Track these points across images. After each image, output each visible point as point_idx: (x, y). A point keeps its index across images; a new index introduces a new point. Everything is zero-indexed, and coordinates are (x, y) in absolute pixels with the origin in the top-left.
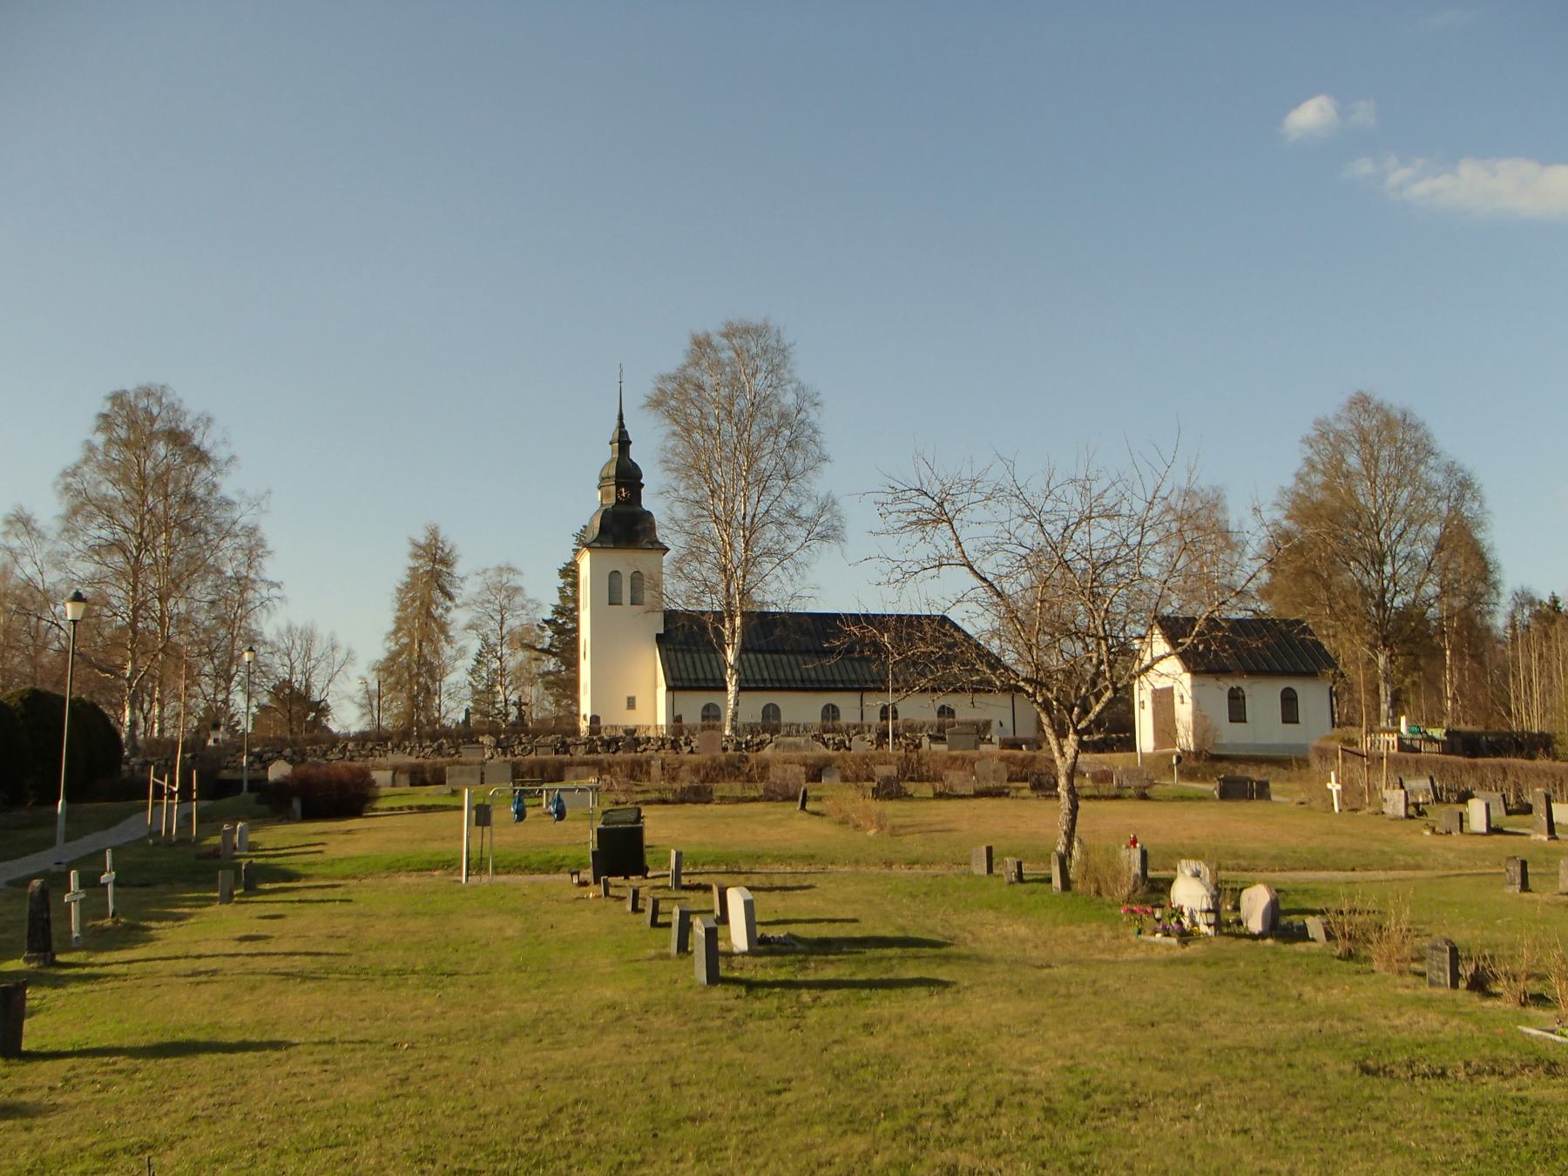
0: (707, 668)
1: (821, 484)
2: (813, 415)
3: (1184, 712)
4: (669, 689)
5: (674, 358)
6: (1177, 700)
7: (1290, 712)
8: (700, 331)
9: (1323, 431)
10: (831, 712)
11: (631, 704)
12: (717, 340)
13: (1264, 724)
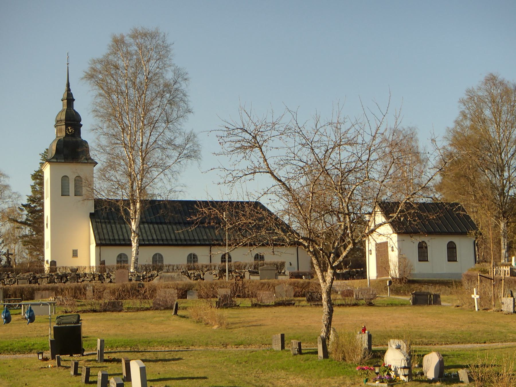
0: (120, 233)
2: (183, 86)
3: (393, 256)
4: (97, 245)
5: (101, 49)
6: (390, 249)
7: (452, 256)
9: (471, 96)
10: (193, 258)
11: (75, 254)
12: (128, 40)
13: (438, 264)
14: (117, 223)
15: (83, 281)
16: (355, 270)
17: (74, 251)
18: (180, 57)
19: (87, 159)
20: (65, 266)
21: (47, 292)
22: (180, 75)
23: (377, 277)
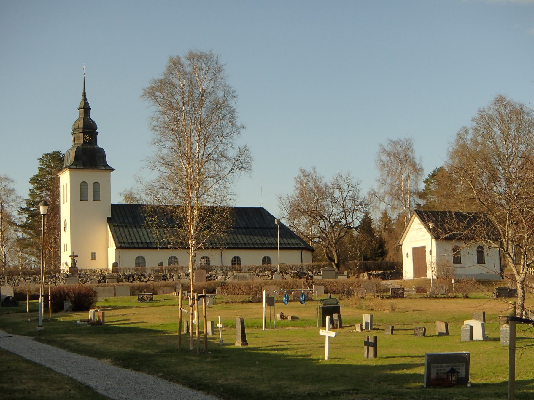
0: (137, 237)
1: (239, 141)
2: (232, 103)
3: (431, 257)
4: (117, 248)
5: (158, 71)
7: (481, 260)
8: (175, 55)
9: (483, 115)
10: (267, 260)
11: (94, 256)
12: (183, 60)
14: (133, 227)
15: (148, 280)
16: (389, 271)
17: (92, 253)
19: (104, 166)
20: (128, 267)
21: (168, 288)
22: (230, 93)
23: (414, 277)
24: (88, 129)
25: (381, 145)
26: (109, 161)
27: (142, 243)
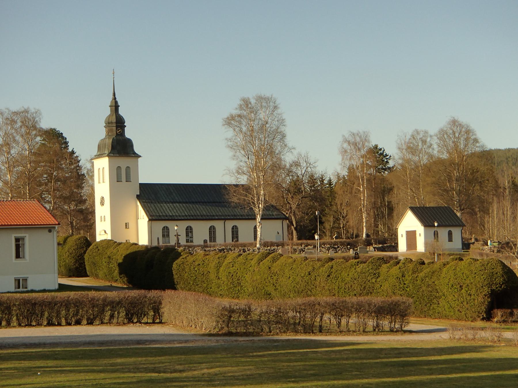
2: (282, 129)
5: (232, 107)
7: (450, 240)
8: (246, 96)
18: (286, 110)
24: (117, 124)
25: (344, 136)
26: (137, 149)
27: (167, 216)
